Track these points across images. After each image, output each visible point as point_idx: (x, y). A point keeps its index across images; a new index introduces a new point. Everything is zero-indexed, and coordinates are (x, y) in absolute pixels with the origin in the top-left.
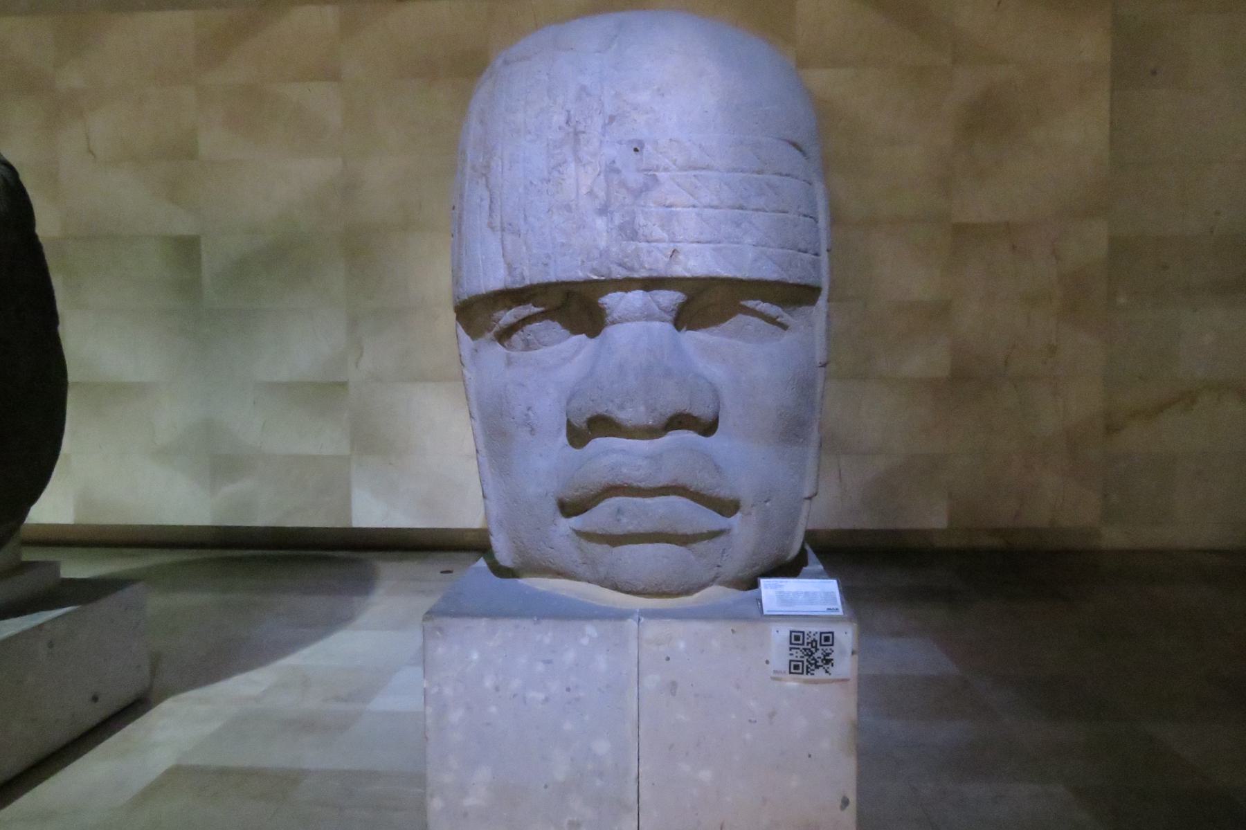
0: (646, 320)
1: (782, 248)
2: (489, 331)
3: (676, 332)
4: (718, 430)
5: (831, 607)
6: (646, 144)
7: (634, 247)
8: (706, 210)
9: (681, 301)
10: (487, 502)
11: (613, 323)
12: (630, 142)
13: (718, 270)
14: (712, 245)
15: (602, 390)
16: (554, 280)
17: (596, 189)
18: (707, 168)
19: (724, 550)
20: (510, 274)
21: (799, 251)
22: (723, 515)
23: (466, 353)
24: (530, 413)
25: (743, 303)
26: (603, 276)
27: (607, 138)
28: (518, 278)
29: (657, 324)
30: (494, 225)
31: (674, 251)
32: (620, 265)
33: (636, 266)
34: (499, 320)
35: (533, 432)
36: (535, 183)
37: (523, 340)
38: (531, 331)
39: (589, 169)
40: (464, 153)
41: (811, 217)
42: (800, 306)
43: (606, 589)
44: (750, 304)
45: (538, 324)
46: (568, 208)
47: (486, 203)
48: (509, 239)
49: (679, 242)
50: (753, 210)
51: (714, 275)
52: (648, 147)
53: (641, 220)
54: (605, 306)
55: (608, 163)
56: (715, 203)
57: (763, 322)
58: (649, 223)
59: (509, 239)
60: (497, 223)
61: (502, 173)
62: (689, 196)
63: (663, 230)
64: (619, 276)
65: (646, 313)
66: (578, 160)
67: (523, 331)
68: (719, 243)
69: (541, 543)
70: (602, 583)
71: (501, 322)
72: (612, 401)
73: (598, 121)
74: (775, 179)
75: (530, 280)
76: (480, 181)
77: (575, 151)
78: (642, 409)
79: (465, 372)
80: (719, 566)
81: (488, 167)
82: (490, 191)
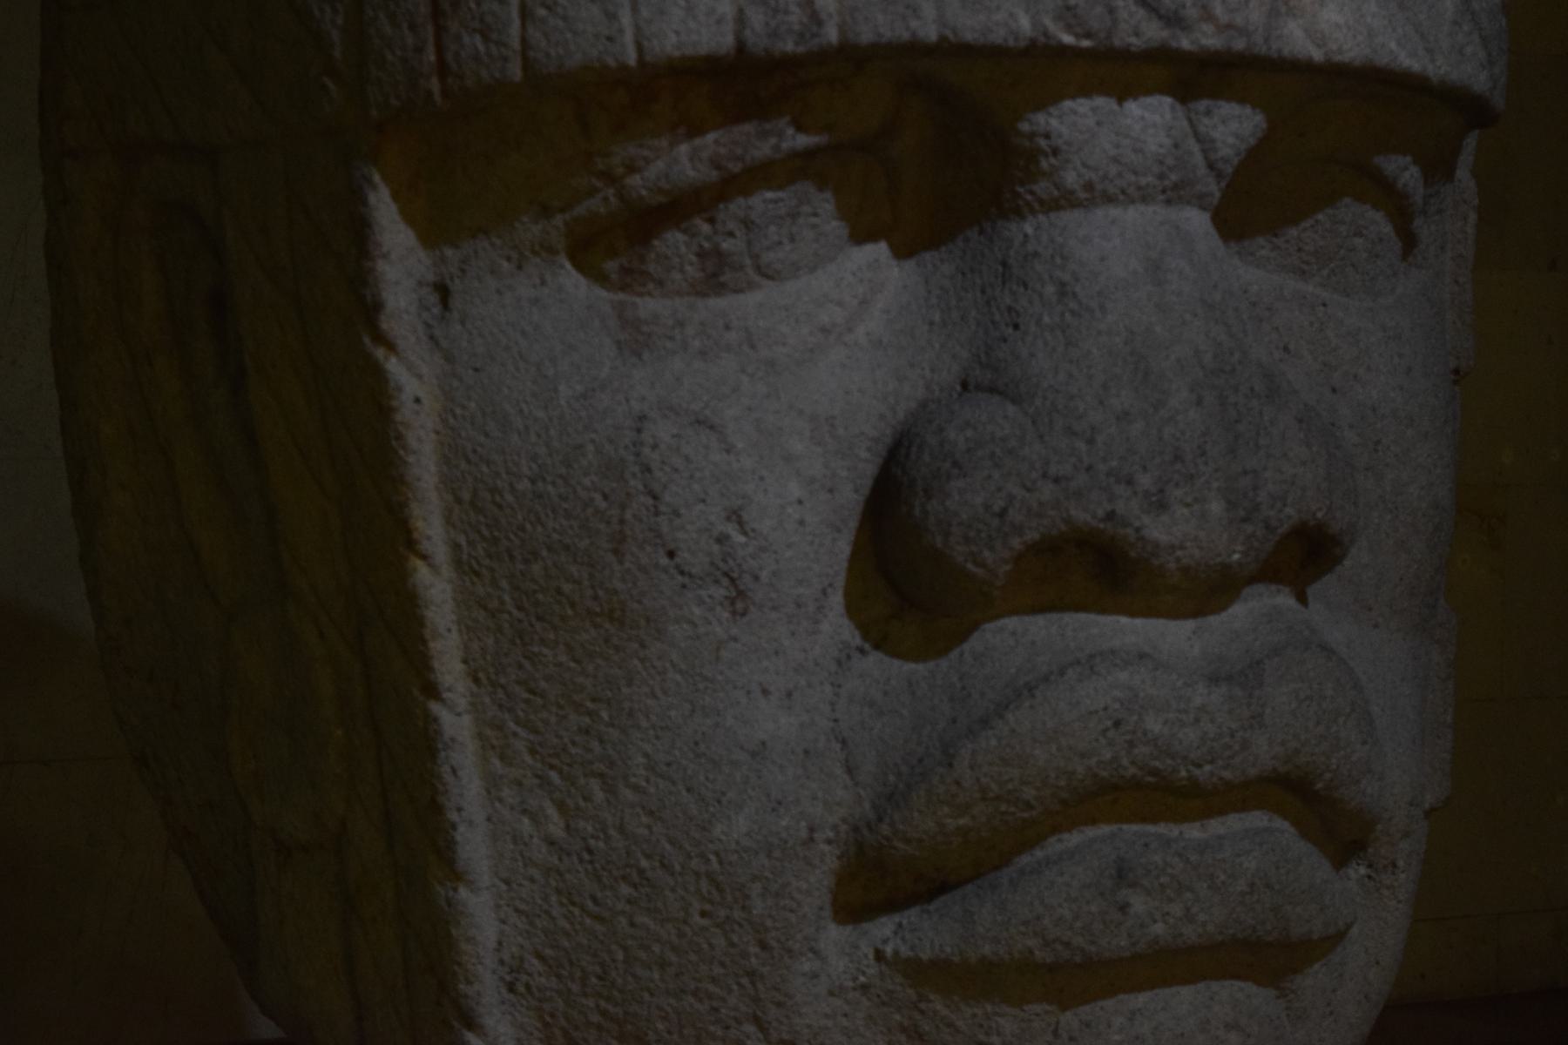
0: (1168, 202)
2: (546, 212)
13: (1393, 45)
16: (930, 33)
26: (1088, 36)
33: (1191, 13)
37: (702, 254)
45: (769, 195)
51: (1382, 60)
54: (1043, 143)
65: (1174, 177)
67: (711, 221)
72: (1130, 482)
75: (842, 28)
78: (1216, 507)
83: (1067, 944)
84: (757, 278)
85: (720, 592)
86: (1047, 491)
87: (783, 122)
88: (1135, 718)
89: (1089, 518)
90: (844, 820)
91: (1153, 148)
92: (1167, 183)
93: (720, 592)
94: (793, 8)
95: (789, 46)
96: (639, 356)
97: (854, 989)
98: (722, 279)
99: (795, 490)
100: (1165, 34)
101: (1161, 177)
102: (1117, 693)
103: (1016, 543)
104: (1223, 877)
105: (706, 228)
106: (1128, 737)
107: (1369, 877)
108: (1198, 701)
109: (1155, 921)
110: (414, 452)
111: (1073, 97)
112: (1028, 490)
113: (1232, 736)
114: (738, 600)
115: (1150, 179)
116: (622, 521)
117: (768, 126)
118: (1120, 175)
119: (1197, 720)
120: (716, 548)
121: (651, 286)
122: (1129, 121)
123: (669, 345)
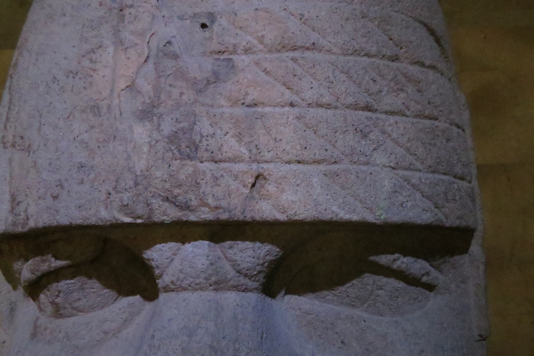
1: (433, 172)
6: (219, 17)
7: (191, 169)
8: (311, 110)
13: (334, 208)
14: (322, 167)
17: (140, 82)
18: (313, 48)
25: (371, 258)
26: (139, 218)
31: (257, 177)
32: (167, 199)
33: (194, 203)
39: (132, 53)
42: (452, 256)
44: (384, 259)
45: (68, 281)
46: (96, 109)
49: (266, 162)
50: (386, 113)
51: (327, 216)
55: (161, 46)
56: (326, 100)
57: (401, 285)
58: (219, 131)
62: (284, 88)
63: (240, 141)
64: (167, 219)
65: (213, 279)
66: (119, 43)
67: (48, 290)
74: (414, 70)
77: (116, 32)
95: (19, 229)
101: (207, 279)
117: (44, 258)
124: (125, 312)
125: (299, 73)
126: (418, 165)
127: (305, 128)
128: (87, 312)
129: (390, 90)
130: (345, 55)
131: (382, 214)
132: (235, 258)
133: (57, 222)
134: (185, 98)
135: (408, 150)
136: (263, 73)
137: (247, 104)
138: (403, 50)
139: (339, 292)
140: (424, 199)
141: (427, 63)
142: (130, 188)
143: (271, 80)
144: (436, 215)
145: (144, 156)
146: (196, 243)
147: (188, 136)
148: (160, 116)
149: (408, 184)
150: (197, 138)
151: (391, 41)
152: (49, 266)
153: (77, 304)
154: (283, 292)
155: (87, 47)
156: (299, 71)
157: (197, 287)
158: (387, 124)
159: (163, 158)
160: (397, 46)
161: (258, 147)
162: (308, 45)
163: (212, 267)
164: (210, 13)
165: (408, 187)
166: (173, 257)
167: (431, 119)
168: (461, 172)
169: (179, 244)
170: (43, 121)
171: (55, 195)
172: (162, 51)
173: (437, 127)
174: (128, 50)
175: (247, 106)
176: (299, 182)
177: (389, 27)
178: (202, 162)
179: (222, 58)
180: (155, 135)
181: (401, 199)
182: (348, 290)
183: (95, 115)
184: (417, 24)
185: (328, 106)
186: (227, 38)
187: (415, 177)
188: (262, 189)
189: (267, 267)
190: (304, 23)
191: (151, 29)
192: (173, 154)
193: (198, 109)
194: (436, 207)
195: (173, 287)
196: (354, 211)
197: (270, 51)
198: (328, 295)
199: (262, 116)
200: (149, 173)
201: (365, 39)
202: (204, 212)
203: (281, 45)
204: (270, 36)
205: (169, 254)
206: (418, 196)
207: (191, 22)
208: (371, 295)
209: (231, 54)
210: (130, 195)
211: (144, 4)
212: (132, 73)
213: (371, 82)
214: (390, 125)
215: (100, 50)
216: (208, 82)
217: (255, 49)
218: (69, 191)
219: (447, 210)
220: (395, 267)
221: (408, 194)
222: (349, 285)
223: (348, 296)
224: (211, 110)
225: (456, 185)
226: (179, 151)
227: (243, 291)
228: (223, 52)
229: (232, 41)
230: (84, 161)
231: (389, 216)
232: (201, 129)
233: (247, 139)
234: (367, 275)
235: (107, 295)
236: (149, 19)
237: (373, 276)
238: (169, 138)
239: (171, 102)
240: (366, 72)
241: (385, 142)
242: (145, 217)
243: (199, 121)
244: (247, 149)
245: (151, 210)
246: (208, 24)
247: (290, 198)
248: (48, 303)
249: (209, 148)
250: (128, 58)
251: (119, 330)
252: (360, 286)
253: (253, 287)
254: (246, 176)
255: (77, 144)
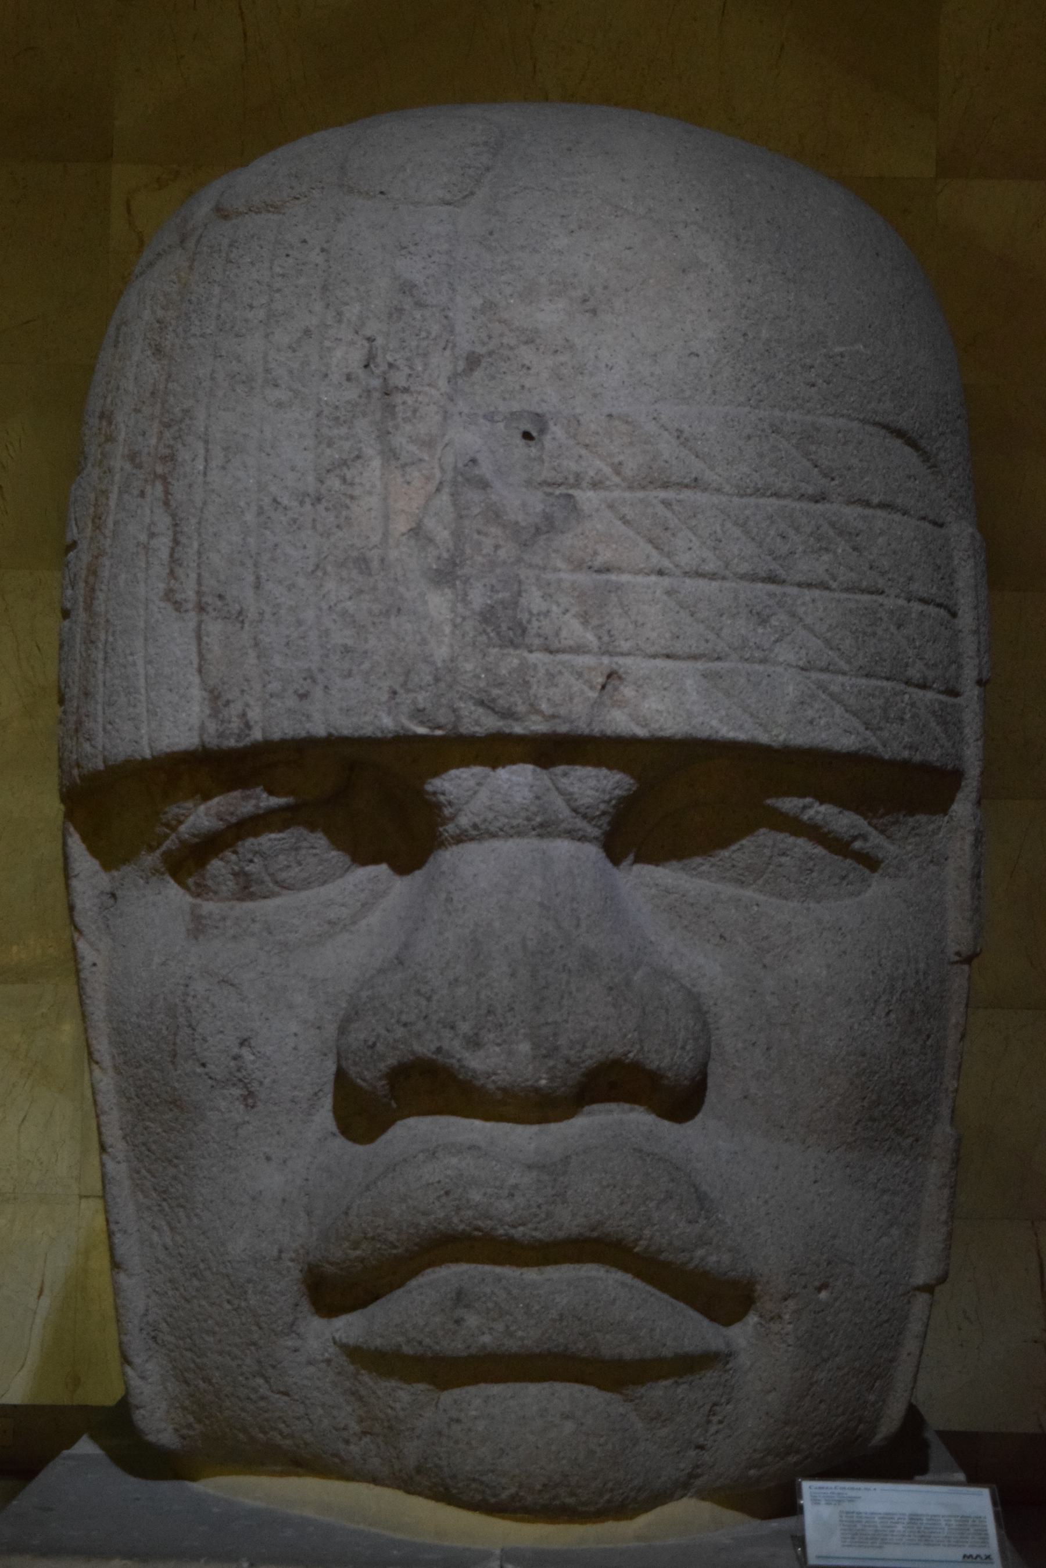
2: (151, 849)
3: (610, 865)
4: (706, 1108)
5: (974, 1552)
6: (551, 423)
7: (516, 661)
8: (688, 581)
9: (625, 793)
10: (122, 1277)
11: (461, 838)
12: (514, 416)
13: (714, 723)
14: (700, 665)
15: (429, 999)
17: (430, 523)
18: (696, 484)
19: (715, 1404)
20: (215, 713)
21: (908, 683)
22: (713, 1319)
23: (86, 901)
24: (245, 1052)
25: (769, 802)
26: (439, 727)
27: (462, 405)
28: (235, 724)
29: (563, 847)
30: (179, 597)
31: (609, 676)
32: (481, 703)
33: (521, 708)
34: (180, 822)
35: (250, 1101)
36: (285, 501)
37: (235, 874)
38: (256, 853)
40: (106, 416)
41: (939, 605)
42: (911, 813)
43: (421, 1499)
44: (789, 804)
45: (273, 836)
47: (163, 544)
48: (214, 628)
49: (622, 654)
50: (799, 585)
51: (704, 733)
52: (557, 431)
53: (534, 600)
54: (442, 798)
55: (460, 465)
56: (709, 567)
57: (819, 851)
58: (554, 608)
59: (214, 628)
60: (189, 593)
61: (205, 474)
63: (585, 623)
64: (479, 731)
65: (539, 819)
66: (390, 455)
67: (235, 852)
68: (719, 659)
69: (260, 1381)
70: (407, 1484)
71: (182, 828)
73: (442, 363)
74: (851, 513)
75: (263, 730)
76: (149, 489)
77: (383, 435)
78: (525, 1047)
79: (82, 945)
80: (701, 1447)
81: (170, 458)
82: (173, 516)
83: (420, 1343)
84: (277, 889)
85: (237, 1092)
86: (400, 1032)
87: (259, 790)
88: (460, 1190)
89: (425, 1051)
90: (302, 1246)
91: (519, 800)
92: (533, 823)
93: (237, 1092)
94: (234, 719)
95: (232, 743)
96: (196, 938)
97: (323, 1361)
98: (252, 889)
99: (294, 1027)
100: (501, 724)
102: (449, 1172)
103: (382, 1066)
104: (537, 1307)
105: (234, 857)
106: (456, 1203)
107: (761, 1324)
108: (512, 1181)
109: (483, 1333)
110: (90, 997)
111: (458, 767)
112: (388, 1030)
113: (539, 1207)
114: (249, 1099)
115: (520, 821)
116: (175, 1044)
117: (248, 792)
118: (496, 818)
119: (511, 1195)
120: (232, 1064)
121: (211, 894)
122: (500, 782)
123: (215, 931)
124: (362, 890)
125: (672, 526)
126: (843, 665)
127: (677, 608)
128: (299, 890)
129: (809, 550)
130: (742, 496)
131: (780, 734)
132: (571, 789)
133: (308, 732)
134: (502, 553)
135: (827, 642)
136: (619, 523)
137: (596, 568)
138: (836, 482)
139: (720, 860)
140: (847, 715)
141: (876, 500)
142: (429, 685)
143: (631, 533)
144: (865, 740)
145: (446, 640)
146: (514, 767)
147: (510, 612)
148: (466, 581)
149: (824, 692)
150: (524, 617)
151: (816, 469)
152: (257, 806)
153: (284, 875)
154: (631, 857)
155: (332, 454)
156: (673, 522)
157: (512, 831)
158: (799, 602)
159: (474, 644)
160: (825, 476)
161: (612, 633)
162: (687, 481)
163: (537, 802)
164: (537, 415)
165: (824, 696)
166: (477, 788)
167: (872, 593)
168: (918, 675)
169: (487, 770)
170: (263, 573)
171: (301, 691)
172: (462, 474)
173: (881, 605)
174: (408, 469)
175: (596, 571)
176: (666, 685)
177: (813, 448)
178: (531, 651)
179: (557, 492)
180: (460, 608)
181: (810, 713)
182: (734, 856)
183: (361, 573)
184: (869, 428)
185: (713, 576)
186: (565, 463)
187: (836, 683)
188: (616, 693)
189: (614, 806)
190: (678, 363)
191: (444, 435)
192: (489, 638)
193: (523, 573)
194: (867, 729)
195: (474, 833)
196: (741, 727)
197: (630, 488)
198: (703, 865)
199: (618, 587)
200: (454, 664)
201: (774, 470)
202: (534, 723)
203: (649, 479)
204: (630, 468)
205: (472, 783)
206: (838, 710)
207: (506, 427)
208: (769, 864)
209: (571, 488)
210: (428, 694)
211: (427, 389)
212: (418, 508)
213: (779, 539)
214: (804, 604)
215: (358, 464)
216: (538, 531)
217: (608, 483)
218: (326, 687)
219: (885, 734)
220: (805, 817)
221: (822, 707)
222: (734, 847)
223: (733, 866)
224: (543, 576)
225: (907, 697)
226: (498, 634)
227: (579, 840)
228: (559, 485)
229: (573, 466)
230: (350, 642)
231: (792, 736)
232: (529, 604)
233: (595, 622)
234: (763, 830)
235: (334, 861)
236: (438, 418)
237: (773, 832)
238: (481, 613)
239: (479, 559)
240: (772, 522)
241: (793, 630)
242: (450, 727)
243: (526, 591)
244: (596, 635)
245: (459, 718)
246: (534, 434)
247: (654, 706)
248: (229, 876)
249: (541, 632)
250: (408, 483)
251: (354, 920)
252: (752, 848)
253: (592, 836)
254: (593, 673)
255: (335, 616)
